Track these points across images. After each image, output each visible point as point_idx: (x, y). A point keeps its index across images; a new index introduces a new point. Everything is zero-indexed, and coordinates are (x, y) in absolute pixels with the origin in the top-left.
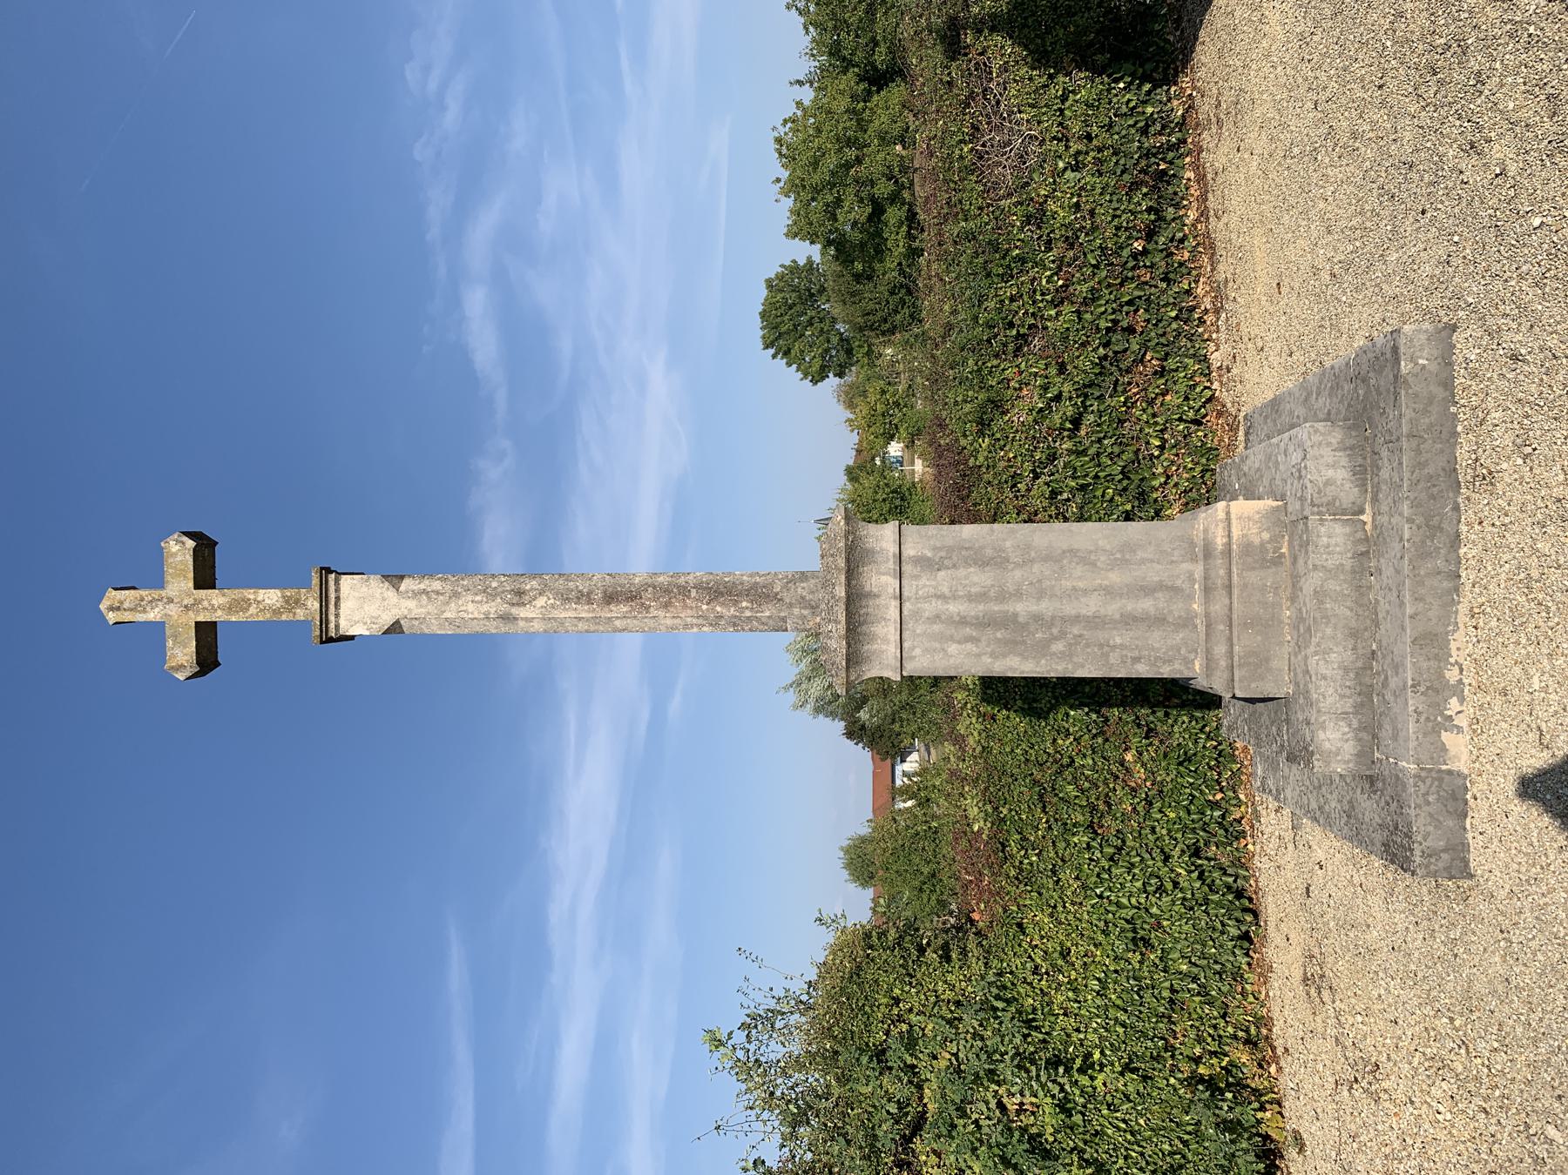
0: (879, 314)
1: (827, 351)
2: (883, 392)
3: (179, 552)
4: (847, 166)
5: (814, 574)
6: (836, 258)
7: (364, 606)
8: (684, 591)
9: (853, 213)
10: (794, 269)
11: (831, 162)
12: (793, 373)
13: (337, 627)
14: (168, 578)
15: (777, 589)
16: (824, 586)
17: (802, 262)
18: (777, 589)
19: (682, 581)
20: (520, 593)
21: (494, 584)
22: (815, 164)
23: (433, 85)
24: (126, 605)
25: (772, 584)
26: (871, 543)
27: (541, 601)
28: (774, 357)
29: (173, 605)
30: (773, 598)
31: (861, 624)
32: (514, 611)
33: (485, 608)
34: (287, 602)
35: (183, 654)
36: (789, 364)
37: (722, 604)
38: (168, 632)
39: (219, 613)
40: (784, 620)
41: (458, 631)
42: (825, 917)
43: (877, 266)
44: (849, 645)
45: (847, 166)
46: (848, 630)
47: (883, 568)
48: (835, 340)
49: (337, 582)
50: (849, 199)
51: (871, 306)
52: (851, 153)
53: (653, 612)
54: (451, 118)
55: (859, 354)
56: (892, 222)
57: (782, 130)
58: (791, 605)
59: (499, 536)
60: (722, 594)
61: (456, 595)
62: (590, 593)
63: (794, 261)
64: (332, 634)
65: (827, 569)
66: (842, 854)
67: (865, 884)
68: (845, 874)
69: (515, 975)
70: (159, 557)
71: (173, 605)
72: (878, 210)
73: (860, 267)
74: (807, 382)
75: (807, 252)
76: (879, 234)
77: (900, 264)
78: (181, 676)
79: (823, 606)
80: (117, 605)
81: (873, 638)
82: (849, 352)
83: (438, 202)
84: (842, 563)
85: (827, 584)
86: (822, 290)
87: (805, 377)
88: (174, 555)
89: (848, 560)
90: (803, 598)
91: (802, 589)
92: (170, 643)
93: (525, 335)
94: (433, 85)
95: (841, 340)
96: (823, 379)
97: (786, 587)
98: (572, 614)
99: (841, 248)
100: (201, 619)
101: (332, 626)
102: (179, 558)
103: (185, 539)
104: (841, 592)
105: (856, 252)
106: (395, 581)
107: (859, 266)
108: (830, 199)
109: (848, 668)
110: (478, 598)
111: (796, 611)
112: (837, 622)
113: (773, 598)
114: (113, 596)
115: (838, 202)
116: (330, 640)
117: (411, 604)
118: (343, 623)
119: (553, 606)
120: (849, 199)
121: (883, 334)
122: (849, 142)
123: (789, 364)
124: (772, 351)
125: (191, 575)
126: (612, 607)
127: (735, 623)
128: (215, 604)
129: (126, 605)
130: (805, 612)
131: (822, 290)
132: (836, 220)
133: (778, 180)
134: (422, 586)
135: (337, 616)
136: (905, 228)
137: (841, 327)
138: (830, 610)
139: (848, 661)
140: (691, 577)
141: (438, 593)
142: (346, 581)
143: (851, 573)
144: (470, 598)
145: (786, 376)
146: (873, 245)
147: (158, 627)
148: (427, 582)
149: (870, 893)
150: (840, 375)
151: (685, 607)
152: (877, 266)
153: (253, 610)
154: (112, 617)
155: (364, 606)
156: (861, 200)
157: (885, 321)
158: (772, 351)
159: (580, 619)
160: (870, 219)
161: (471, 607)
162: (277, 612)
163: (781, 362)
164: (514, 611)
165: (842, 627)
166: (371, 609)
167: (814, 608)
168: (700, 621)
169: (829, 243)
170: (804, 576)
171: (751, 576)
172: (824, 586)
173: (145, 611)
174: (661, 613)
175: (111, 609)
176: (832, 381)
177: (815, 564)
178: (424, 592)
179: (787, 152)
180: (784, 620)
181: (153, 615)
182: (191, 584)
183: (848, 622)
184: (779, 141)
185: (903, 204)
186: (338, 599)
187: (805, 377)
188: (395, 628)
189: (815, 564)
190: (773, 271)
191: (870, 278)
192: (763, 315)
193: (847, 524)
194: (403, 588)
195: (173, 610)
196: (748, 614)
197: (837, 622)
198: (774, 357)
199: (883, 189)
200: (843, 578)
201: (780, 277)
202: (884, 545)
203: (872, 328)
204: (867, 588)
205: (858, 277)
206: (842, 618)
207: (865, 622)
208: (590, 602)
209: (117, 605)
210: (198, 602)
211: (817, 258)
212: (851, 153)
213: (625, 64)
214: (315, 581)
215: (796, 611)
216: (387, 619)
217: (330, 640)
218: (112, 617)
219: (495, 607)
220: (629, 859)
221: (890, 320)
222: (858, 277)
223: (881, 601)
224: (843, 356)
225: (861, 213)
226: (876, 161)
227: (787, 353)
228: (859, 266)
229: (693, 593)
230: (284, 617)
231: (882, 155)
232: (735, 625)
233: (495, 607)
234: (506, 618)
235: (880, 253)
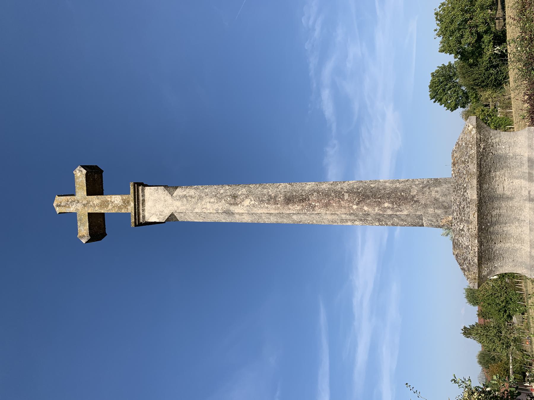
0: (480, 80)
1: (457, 98)
2: (483, 111)
3: (80, 174)
4: (466, 21)
5: (446, 181)
6: (461, 59)
7: (157, 204)
8: (339, 195)
9: (468, 39)
10: (443, 67)
11: (460, 18)
12: (443, 108)
13: (144, 217)
14: (77, 190)
15: (414, 192)
16: (456, 190)
17: (447, 64)
18: (414, 192)
19: (338, 187)
20: (235, 197)
21: (222, 191)
22: (452, 22)
23: (311, 23)
24: (63, 204)
25: (409, 189)
26: (502, 150)
27: (247, 202)
28: (435, 102)
29: (80, 204)
30: (413, 200)
31: (493, 224)
32: (233, 208)
33: (216, 206)
34: (124, 202)
35: (83, 230)
36: (441, 104)
37: (368, 205)
38: (78, 218)
39: (97, 208)
40: (420, 217)
41: (205, 220)
42: (458, 379)
43: (479, 60)
44: (481, 243)
45: (466, 21)
46: (480, 229)
47: (516, 173)
48: (461, 94)
49: (143, 191)
50: (467, 34)
51: (477, 76)
52: (468, 16)
53: (318, 210)
54: (317, 33)
55: (471, 98)
56: (486, 41)
57: (439, 10)
58: (426, 206)
59: (333, 173)
60: (368, 197)
61: (200, 198)
62: (275, 197)
63: (443, 65)
64: (141, 221)
65: (459, 174)
66: (464, 291)
67: (474, 305)
68: (466, 300)
69: (342, 321)
70: (72, 178)
71: (80, 204)
72: (480, 37)
73: (472, 61)
74: (449, 111)
75: (450, 59)
76: (480, 46)
77: (490, 58)
78: (84, 241)
79: (454, 207)
80: (61, 204)
81: (506, 237)
82: (467, 98)
83: (313, 62)
84: (473, 168)
85: (458, 187)
86: (455, 74)
87: (448, 108)
88: (79, 178)
89: (479, 166)
90: (436, 200)
91: (436, 193)
92: (79, 224)
93: (343, 104)
94: (311, 23)
95: (464, 93)
96: (455, 109)
97: (422, 191)
98: (265, 211)
99: (463, 55)
100: (90, 211)
101: (141, 216)
102: (80, 179)
103: (82, 169)
104: (472, 194)
105: (469, 56)
106: (171, 189)
107: (471, 61)
108: (458, 35)
109: (480, 264)
110: (212, 200)
111: (431, 211)
112: (468, 222)
113: (413, 200)
114: (58, 200)
115: (462, 36)
116: (141, 224)
117: (178, 203)
118: (147, 215)
119: (254, 206)
120: (467, 34)
121: (483, 87)
122: (466, 12)
123: (441, 104)
124: (434, 100)
125: (85, 188)
126: (290, 206)
127: (380, 219)
128: (96, 204)
129: (63, 204)
130: (439, 212)
131: (455, 74)
132: (461, 43)
133: (436, 30)
134: (185, 193)
135: (143, 210)
136: (492, 43)
137: (464, 88)
138: (462, 211)
139: (480, 258)
140: (345, 184)
141: (191, 197)
142: (148, 190)
143: (483, 177)
144: (208, 200)
145: (440, 109)
146: (478, 50)
147: (74, 215)
148: (188, 190)
149: (476, 308)
150: (464, 107)
151: (340, 207)
152: (479, 60)
153: (110, 207)
154: (58, 210)
155: (157, 204)
156: (472, 34)
157: (483, 82)
158: (434, 100)
159: (271, 214)
160: (476, 41)
161: (208, 206)
162: (120, 208)
163: (437, 104)
164: (233, 208)
165: (474, 227)
166: (159, 207)
167: (446, 208)
168: (352, 217)
169: (458, 53)
170: (437, 182)
171: (392, 182)
172: (456, 190)
173: (69, 207)
174: (323, 211)
175: (58, 206)
176: (460, 110)
177: (446, 171)
178: (185, 196)
179: (440, 18)
180: (420, 217)
181: (72, 209)
182: (85, 193)
183: (480, 223)
184: (436, 14)
185: (491, 33)
186: (144, 201)
187: (448, 108)
188: (172, 218)
189: (446, 171)
190: (434, 69)
191: (476, 65)
192: (430, 87)
193: (480, 133)
194: (175, 194)
195: (79, 206)
196: (389, 212)
197: (468, 222)
198: (435, 102)
199: (482, 29)
200: (475, 182)
201: (437, 72)
202: (518, 151)
203: (477, 85)
204: (500, 191)
205: (471, 65)
206: (474, 217)
207: (497, 222)
208: (276, 203)
209: (61, 204)
210: (88, 202)
211: (453, 62)
212: (468, 16)
213: (377, 4)
214: (132, 191)
215: (431, 211)
216: (167, 214)
217: (141, 224)
218: (58, 210)
219: (222, 206)
220: (381, 286)
221: (486, 81)
222: (471, 65)
223: (515, 203)
224: (464, 100)
225: (472, 40)
226: (479, 17)
227: (440, 100)
228: (471, 61)
229: (346, 196)
230: (123, 211)
231: (482, 15)
232: (379, 220)
233: (222, 206)
234: (228, 213)
235: (481, 55)
